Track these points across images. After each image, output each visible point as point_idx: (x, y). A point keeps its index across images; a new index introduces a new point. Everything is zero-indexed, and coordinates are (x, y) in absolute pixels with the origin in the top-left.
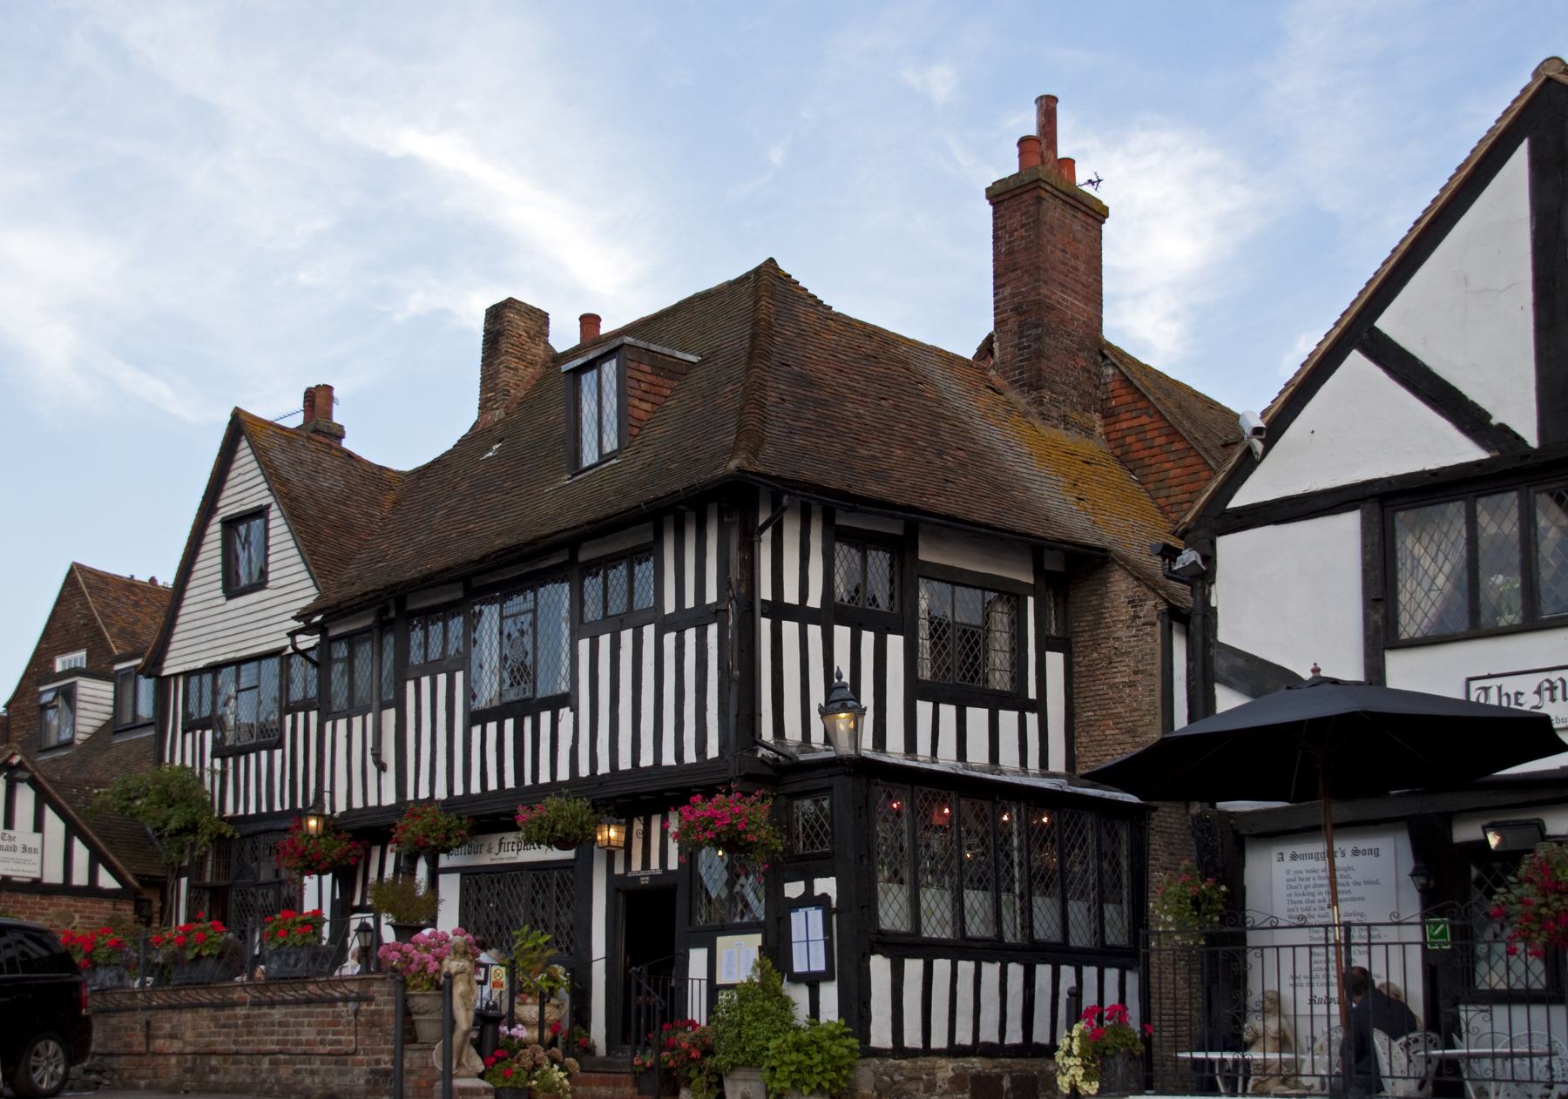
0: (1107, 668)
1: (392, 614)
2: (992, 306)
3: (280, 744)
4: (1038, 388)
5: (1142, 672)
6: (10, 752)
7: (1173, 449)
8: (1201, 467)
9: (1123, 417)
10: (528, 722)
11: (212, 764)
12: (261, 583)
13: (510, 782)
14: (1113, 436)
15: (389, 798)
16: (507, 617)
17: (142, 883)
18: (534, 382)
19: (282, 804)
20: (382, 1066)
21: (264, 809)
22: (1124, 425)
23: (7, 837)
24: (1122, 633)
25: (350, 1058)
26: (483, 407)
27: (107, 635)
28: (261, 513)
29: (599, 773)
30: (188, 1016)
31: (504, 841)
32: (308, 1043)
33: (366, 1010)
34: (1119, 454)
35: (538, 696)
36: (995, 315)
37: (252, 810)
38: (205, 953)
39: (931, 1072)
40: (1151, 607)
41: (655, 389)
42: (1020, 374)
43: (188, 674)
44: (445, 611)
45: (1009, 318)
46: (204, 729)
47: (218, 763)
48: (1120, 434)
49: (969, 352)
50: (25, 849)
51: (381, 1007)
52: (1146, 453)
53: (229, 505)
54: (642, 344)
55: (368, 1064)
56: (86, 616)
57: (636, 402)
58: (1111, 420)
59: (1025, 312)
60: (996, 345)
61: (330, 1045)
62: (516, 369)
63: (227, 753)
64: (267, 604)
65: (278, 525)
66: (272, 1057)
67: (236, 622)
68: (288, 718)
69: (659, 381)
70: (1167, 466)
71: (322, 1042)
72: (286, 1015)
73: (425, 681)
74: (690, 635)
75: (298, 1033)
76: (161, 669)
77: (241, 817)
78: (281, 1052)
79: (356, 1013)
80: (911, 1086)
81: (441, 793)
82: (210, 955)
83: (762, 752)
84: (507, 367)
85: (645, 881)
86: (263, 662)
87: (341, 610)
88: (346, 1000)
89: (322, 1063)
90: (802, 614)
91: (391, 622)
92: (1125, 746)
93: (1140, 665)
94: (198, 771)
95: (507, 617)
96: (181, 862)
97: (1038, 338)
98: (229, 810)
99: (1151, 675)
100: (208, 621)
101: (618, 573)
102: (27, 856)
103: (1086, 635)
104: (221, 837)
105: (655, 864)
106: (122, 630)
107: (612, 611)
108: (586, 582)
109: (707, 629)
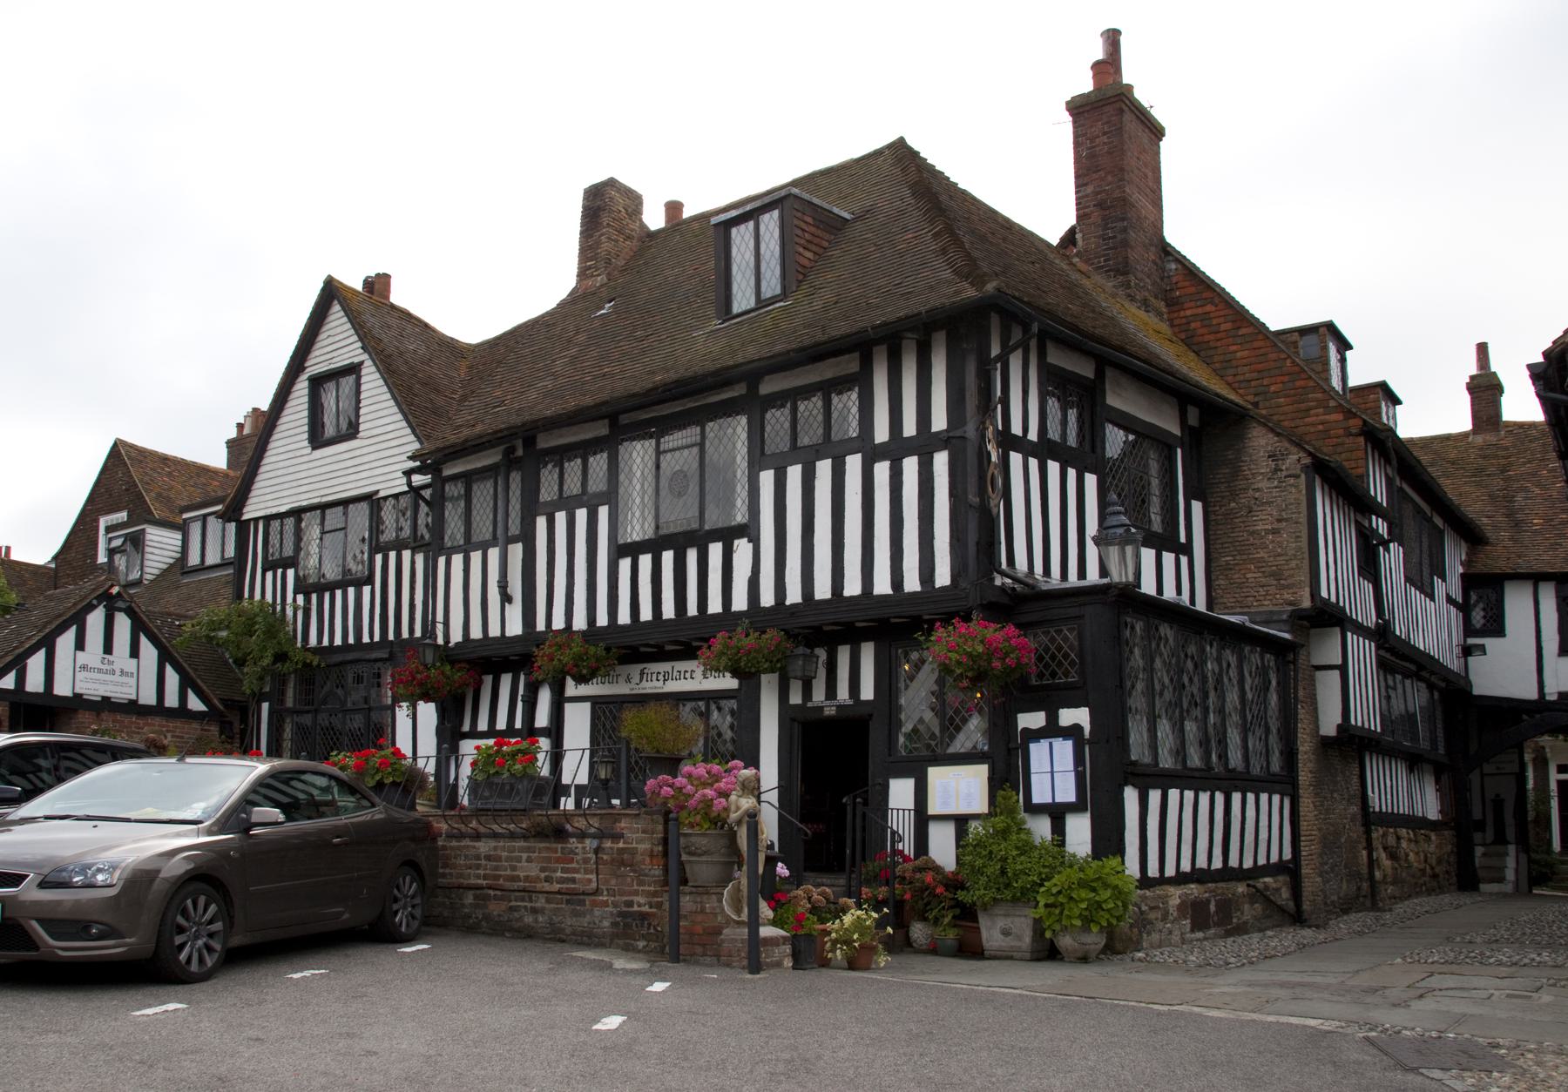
0: (1247, 516)
1: (520, 452)
2: (1074, 202)
4: (1125, 273)
5: (1286, 520)
6: (110, 583)
7: (1240, 333)
8: (1269, 349)
9: (1186, 306)
10: (692, 556)
11: (295, 600)
12: (352, 432)
13: (669, 611)
14: (1176, 322)
15: (515, 628)
16: (665, 452)
17: (226, 706)
18: (632, 254)
19: (371, 636)
20: (636, 908)
21: (351, 640)
22: (1188, 313)
23: (106, 661)
24: (1264, 484)
25: (588, 899)
26: (583, 274)
27: (147, 498)
28: (354, 369)
29: (788, 602)
31: (646, 671)
32: (527, 878)
33: (611, 848)
34: (1184, 337)
35: (707, 527)
36: (1077, 210)
37: (338, 641)
38: (388, 780)
39: (1165, 899)
40: (1294, 460)
41: (816, 240)
42: (1105, 261)
43: (268, 519)
44: (585, 450)
45: (1092, 212)
46: (285, 568)
47: (300, 599)
48: (1184, 321)
50: (122, 672)
51: (634, 845)
52: (1212, 337)
53: (319, 362)
54: (806, 196)
55: (615, 905)
56: (128, 483)
57: (801, 250)
58: (1175, 308)
59: (1109, 208)
60: (1079, 236)
61: (558, 883)
62: (617, 241)
63: (310, 589)
64: (358, 453)
66: (478, 892)
67: (323, 470)
68: (379, 558)
69: (819, 232)
70: (1233, 348)
71: (547, 880)
72: (495, 848)
73: (561, 518)
75: (514, 868)
76: (242, 514)
78: (490, 888)
79: (597, 851)
80: (1152, 916)
82: (394, 784)
84: (609, 238)
85: (830, 711)
86: (351, 506)
87: (466, 449)
89: (548, 901)
91: (518, 461)
92: (1269, 588)
93: (1284, 513)
94: (279, 608)
95: (665, 452)
96: (261, 689)
97: (1125, 230)
98: (313, 641)
99: (1297, 523)
100: (291, 470)
101: (811, 405)
102: (124, 679)
103: (1223, 487)
104: (307, 665)
105: (843, 693)
106: (159, 495)
107: (804, 440)
108: (768, 415)
109: (932, 457)
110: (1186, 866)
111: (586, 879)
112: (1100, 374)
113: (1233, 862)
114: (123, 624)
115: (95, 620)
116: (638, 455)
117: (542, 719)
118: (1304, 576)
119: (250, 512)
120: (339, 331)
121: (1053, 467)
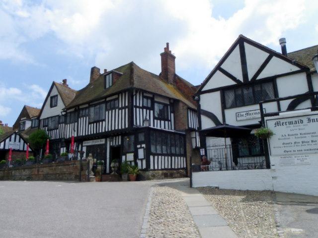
3: (58, 129)
10: (98, 124)
26: (90, 81)
28: (57, 96)
30: (45, 168)
43: (44, 119)
44: (86, 108)
49: (158, 75)
53: (52, 94)
54: (117, 72)
65: (59, 97)
74: (123, 110)
77: (58, 139)
81: (84, 134)
83: (134, 126)
85: (116, 146)
88: (71, 164)
90: (139, 107)
105: (117, 143)
110: (163, 168)
111: (72, 171)
112: (154, 96)
113: (173, 167)
114: (18, 137)
115: (13, 136)
116: (92, 109)
117: (80, 149)
118: (186, 124)
119: (42, 118)
120: (55, 90)
121: (145, 110)
